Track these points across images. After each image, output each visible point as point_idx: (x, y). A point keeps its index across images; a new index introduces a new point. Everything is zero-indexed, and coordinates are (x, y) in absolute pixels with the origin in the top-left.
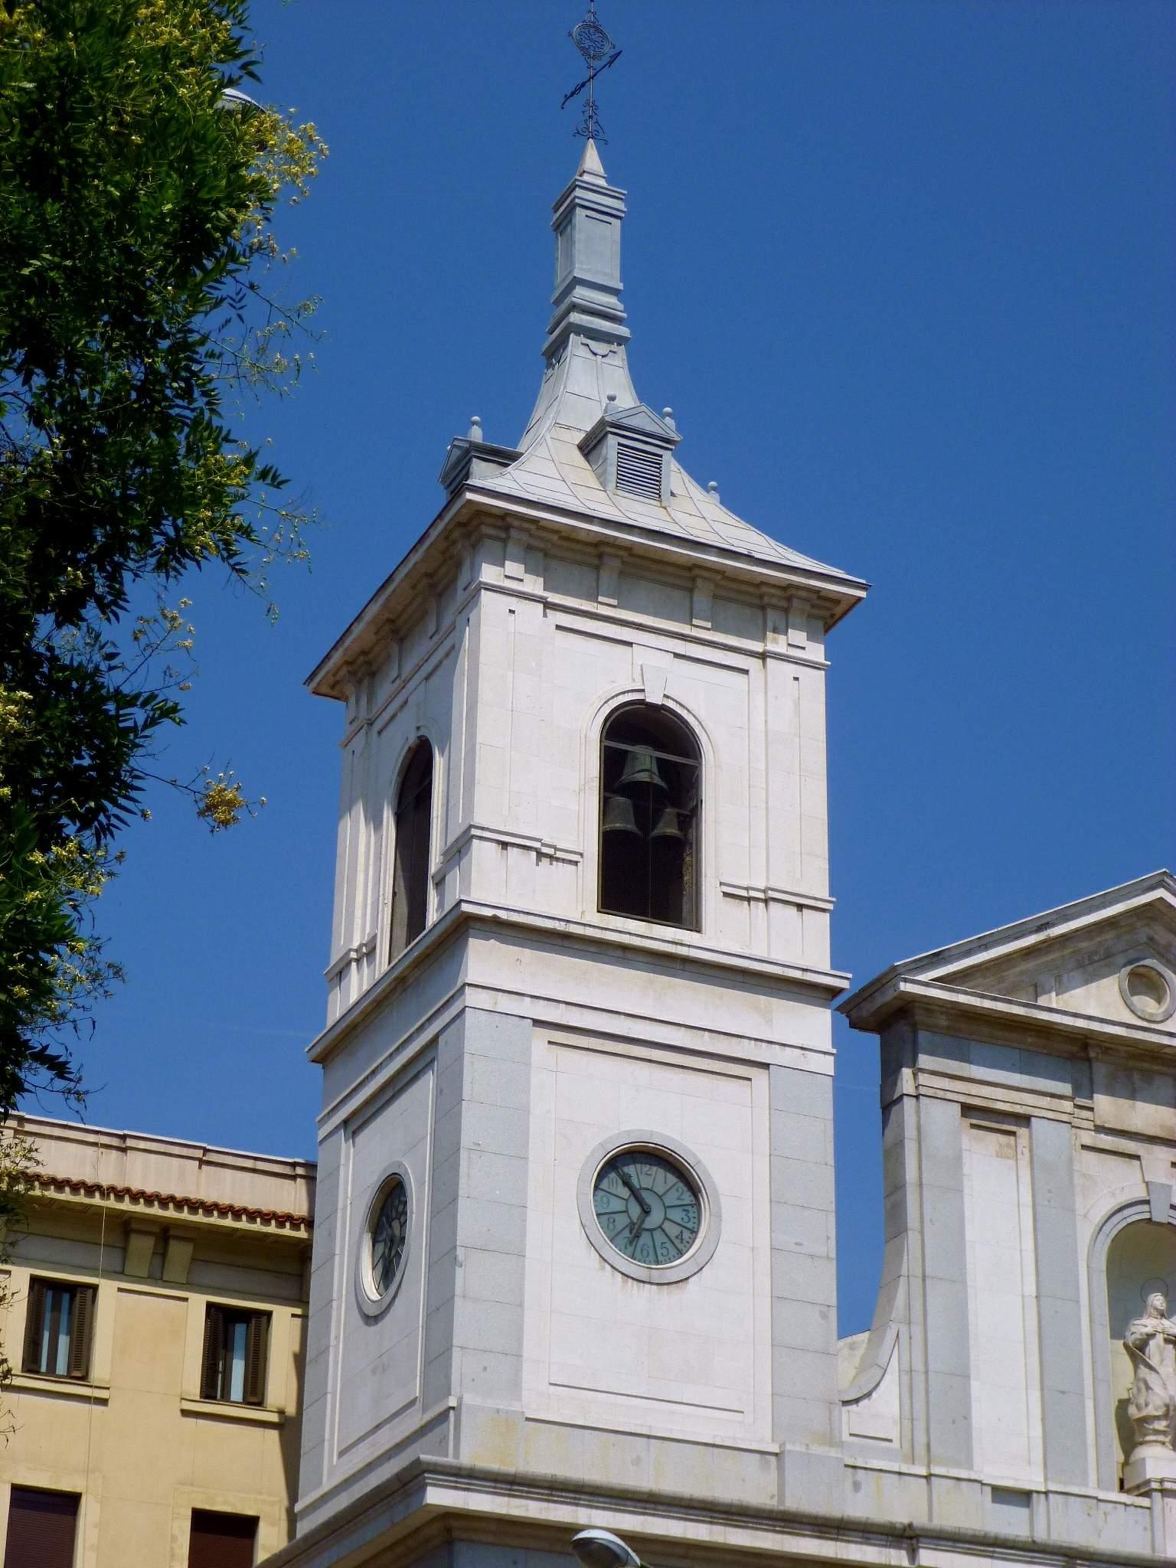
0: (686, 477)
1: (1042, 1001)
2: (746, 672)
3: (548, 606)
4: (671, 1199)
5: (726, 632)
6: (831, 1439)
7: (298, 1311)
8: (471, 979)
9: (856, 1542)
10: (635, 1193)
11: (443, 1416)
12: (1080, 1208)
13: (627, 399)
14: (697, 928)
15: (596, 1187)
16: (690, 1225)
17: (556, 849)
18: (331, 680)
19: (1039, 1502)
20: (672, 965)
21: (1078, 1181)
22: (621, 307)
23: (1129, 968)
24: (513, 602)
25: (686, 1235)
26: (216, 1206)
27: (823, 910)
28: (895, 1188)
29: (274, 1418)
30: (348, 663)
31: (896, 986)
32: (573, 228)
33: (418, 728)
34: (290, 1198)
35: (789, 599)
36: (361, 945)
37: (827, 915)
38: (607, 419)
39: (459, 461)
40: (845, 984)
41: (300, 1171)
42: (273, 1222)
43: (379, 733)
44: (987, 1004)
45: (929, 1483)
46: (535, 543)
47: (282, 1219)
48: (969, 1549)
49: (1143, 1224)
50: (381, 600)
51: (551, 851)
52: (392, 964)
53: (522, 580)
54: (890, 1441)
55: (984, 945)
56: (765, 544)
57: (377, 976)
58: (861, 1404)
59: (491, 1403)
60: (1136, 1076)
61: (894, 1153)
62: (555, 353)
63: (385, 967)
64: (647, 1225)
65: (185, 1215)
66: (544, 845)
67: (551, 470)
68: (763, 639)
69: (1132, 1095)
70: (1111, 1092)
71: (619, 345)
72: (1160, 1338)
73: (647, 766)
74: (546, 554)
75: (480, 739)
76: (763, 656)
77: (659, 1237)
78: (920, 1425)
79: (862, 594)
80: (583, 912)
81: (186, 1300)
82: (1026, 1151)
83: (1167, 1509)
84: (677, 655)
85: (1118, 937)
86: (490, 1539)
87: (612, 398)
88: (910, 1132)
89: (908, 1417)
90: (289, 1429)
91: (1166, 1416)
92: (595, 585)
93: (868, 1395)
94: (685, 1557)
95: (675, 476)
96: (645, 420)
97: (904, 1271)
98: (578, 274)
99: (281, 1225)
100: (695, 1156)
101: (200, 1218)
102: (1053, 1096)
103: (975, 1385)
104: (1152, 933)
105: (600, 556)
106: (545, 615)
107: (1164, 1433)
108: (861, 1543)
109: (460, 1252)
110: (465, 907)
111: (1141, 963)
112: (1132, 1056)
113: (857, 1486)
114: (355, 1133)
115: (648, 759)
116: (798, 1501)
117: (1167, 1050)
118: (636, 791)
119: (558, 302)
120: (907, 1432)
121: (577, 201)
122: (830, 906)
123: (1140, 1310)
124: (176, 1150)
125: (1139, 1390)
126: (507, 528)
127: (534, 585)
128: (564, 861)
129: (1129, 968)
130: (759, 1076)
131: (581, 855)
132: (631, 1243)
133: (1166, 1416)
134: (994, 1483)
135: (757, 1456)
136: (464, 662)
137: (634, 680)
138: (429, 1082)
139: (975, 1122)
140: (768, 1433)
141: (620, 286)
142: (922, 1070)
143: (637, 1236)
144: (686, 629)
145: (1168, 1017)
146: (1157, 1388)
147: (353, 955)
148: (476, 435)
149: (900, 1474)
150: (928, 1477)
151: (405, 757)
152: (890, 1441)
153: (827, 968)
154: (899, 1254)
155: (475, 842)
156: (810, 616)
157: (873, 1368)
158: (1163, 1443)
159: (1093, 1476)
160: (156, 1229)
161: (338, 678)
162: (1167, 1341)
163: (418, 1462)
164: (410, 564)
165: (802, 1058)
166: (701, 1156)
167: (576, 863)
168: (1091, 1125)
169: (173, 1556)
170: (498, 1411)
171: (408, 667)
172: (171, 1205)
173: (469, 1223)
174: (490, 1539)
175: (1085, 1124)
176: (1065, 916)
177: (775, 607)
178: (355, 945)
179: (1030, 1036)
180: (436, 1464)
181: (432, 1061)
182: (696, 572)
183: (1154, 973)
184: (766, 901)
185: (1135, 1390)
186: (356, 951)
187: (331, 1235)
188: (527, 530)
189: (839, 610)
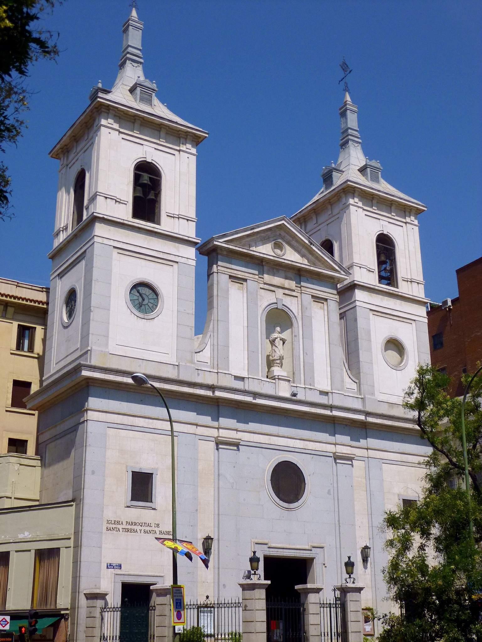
0: (159, 102)
1: (251, 249)
2: (174, 155)
3: (120, 132)
4: (150, 297)
5: (170, 143)
6: (192, 362)
7: (43, 327)
8: (96, 234)
9: (199, 389)
10: (141, 295)
11: (86, 353)
13: (142, 78)
14: (159, 224)
17: (121, 200)
18: (56, 153)
19: (246, 380)
22: (141, 54)
23: (274, 241)
24: (110, 130)
25: (154, 306)
26: (21, 298)
27: (194, 221)
28: (211, 296)
29: (36, 356)
31: (213, 243)
32: (128, 32)
33: (81, 166)
34: (42, 297)
35: (187, 136)
36: (64, 226)
37: (195, 223)
38: (138, 83)
39: (95, 93)
40: (199, 241)
41: (44, 290)
42: (37, 303)
44: (237, 249)
45: (218, 374)
46: (117, 114)
47: (39, 302)
49: (275, 309)
50: (72, 129)
51: (119, 200)
52: (73, 231)
53: (113, 125)
54: (208, 363)
55: (237, 233)
56: (180, 120)
57: (68, 235)
60: (275, 270)
61: (210, 288)
62: (122, 65)
63: (70, 232)
64: (144, 303)
65: (12, 300)
66: (117, 198)
67: (121, 95)
68: (179, 146)
69: (274, 275)
70: (268, 274)
71: (140, 64)
72: (279, 339)
73: (147, 179)
74: (120, 118)
75: (100, 168)
76: (179, 151)
77: (147, 306)
79: (207, 135)
80: (128, 218)
81: (12, 323)
82: (246, 288)
83: (279, 383)
84: (155, 149)
87: (139, 77)
88: (215, 282)
89: (212, 357)
90: (41, 359)
92: (133, 127)
95: (156, 101)
96: (148, 83)
97: (212, 319)
98: (129, 44)
99: (39, 303)
101: (16, 301)
102: (253, 274)
103: (230, 349)
105: (135, 119)
106: (119, 135)
108: (200, 389)
109: (92, 308)
110: (95, 214)
111: (277, 241)
112: (274, 265)
113: (198, 374)
114: (61, 278)
115: (146, 177)
116: (182, 377)
117: (283, 264)
118: (143, 186)
119: (123, 52)
120: (212, 360)
122: (196, 220)
123: (274, 331)
124: (10, 282)
125: (273, 352)
126: (109, 110)
127: (116, 126)
128: (123, 203)
129: (274, 241)
130: (175, 265)
136: (96, 146)
137: (143, 155)
138: (83, 263)
139: (232, 280)
142: (219, 266)
143: (141, 306)
144: (158, 142)
145: (284, 255)
146: (277, 352)
147: (61, 229)
148: (100, 85)
149: (210, 371)
150: (217, 373)
151: (77, 175)
152: (208, 363)
154: (211, 314)
155: (98, 196)
156: (192, 141)
157: (203, 344)
158: (279, 366)
160: (4, 304)
161: (58, 152)
162: (280, 340)
163: (80, 363)
164: (80, 120)
166: (159, 286)
167: (126, 204)
168: (263, 282)
169: (8, 392)
170: (102, 351)
171: (79, 149)
172: (8, 297)
173: (95, 301)
175: (261, 282)
176: (258, 226)
177: (183, 138)
178: (62, 226)
180: (85, 364)
181: (84, 257)
182: (162, 126)
183: (280, 243)
184: (178, 218)
185: (272, 352)
187: (54, 305)
188: (115, 111)
189: (201, 139)
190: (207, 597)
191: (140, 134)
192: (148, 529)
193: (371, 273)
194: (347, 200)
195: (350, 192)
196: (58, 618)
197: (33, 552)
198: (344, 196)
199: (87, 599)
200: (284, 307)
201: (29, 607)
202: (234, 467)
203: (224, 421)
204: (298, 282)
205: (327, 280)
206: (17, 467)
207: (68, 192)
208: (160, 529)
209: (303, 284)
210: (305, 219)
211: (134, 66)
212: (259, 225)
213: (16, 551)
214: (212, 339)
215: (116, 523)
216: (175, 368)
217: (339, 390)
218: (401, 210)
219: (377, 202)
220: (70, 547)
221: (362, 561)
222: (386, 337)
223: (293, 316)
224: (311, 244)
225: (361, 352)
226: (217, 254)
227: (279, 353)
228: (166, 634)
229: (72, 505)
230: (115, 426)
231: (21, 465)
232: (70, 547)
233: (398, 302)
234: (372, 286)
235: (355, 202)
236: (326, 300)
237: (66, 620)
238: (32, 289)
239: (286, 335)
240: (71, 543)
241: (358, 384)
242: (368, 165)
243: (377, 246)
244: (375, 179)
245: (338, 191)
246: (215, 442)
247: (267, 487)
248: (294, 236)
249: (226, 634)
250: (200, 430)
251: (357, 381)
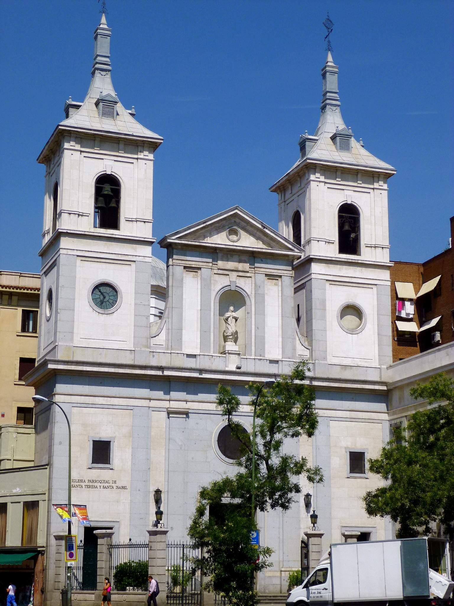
2: (133, 163)
10: (102, 293)
11: (55, 348)
12: (212, 288)
15: (92, 293)
16: (115, 300)
19: (198, 357)
21: (212, 282)
25: (114, 302)
27: (151, 222)
30: (45, 157)
35: (144, 144)
36: (47, 230)
43: (51, 176)
44: (190, 243)
55: (189, 228)
59: (65, 344)
60: (229, 256)
65: (15, 290)
69: (228, 261)
70: (222, 260)
74: (81, 138)
77: (108, 303)
78: (170, 341)
79: (162, 141)
82: (200, 276)
83: (229, 357)
85: (227, 222)
86: (64, 374)
89: (167, 340)
91: (232, 335)
93: (158, 335)
94: (110, 375)
98: (98, 53)
100: (116, 284)
101: (18, 291)
102: (207, 262)
104: (235, 220)
107: (232, 339)
110: (59, 230)
113: (153, 356)
118: (106, 197)
121: (98, 33)
122: (152, 221)
124: (14, 274)
127: (78, 147)
128: (85, 216)
131: (90, 214)
132: (101, 305)
133: (232, 335)
135: (129, 351)
138: (55, 269)
140: (132, 346)
141: (109, 55)
143: (102, 303)
147: (46, 232)
149: (164, 353)
153: (151, 237)
159: (212, 350)
163: (46, 359)
166: (118, 284)
167: (88, 216)
168: (217, 268)
169: (15, 369)
170: (67, 346)
174: (64, 374)
175: (215, 268)
177: (140, 146)
186: (47, 231)
190: (130, 540)
191: (100, 150)
192: (106, 485)
193: (331, 245)
194: (309, 176)
195: (312, 168)
196: (36, 553)
197: (22, 503)
198: (307, 171)
199: (56, 539)
200: (236, 287)
201: (20, 545)
202: (183, 432)
203: (174, 394)
204: (252, 264)
205: (282, 258)
206: (15, 435)
207: (50, 198)
209: (257, 265)
210: (284, 187)
211: (102, 75)
212: (212, 218)
213: (12, 503)
214: (167, 324)
215: (80, 481)
216: (131, 353)
217: (289, 358)
218: (369, 176)
219: (342, 173)
220: (45, 500)
221: (305, 506)
222: (342, 304)
223: (246, 295)
224: (264, 228)
225: (314, 321)
226: (173, 249)
227: (231, 330)
228: (104, 566)
229: (46, 468)
230: (79, 405)
231: (18, 433)
232: (45, 500)
233: (359, 269)
234: (328, 258)
235: (316, 178)
236: (280, 277)
237: (43, 555)
238: (33, 277)
239: (239, 314)
240: (46, 497)
241: (311, 350)
242: (338, 134)
243: (340, 217)
244: (345, 147)
245: (302, 167)
246: (166, 412)
247: (214, 447)
248: (248, 223)
249: (170, 566)
250: (153, 403)
251: (310, 348)
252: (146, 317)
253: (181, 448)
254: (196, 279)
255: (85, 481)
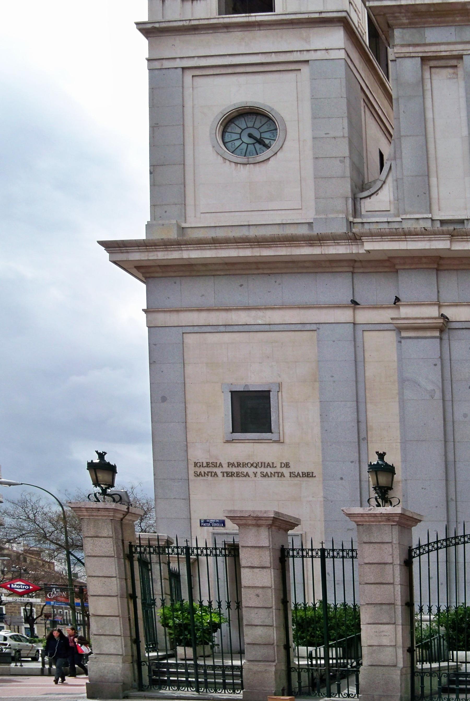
20: (254, 29)
48: (391, 238)
58: (372, 197)
134: (441, 219)
165: (327, 54)
179: (457, 17)
192: (269, 470)
208: (292, 470)
215: (210, 465)
230: (196, 329)
252: (338, 159)
253: (432, 397)
254: (455, 80)
255: (221, 464)
